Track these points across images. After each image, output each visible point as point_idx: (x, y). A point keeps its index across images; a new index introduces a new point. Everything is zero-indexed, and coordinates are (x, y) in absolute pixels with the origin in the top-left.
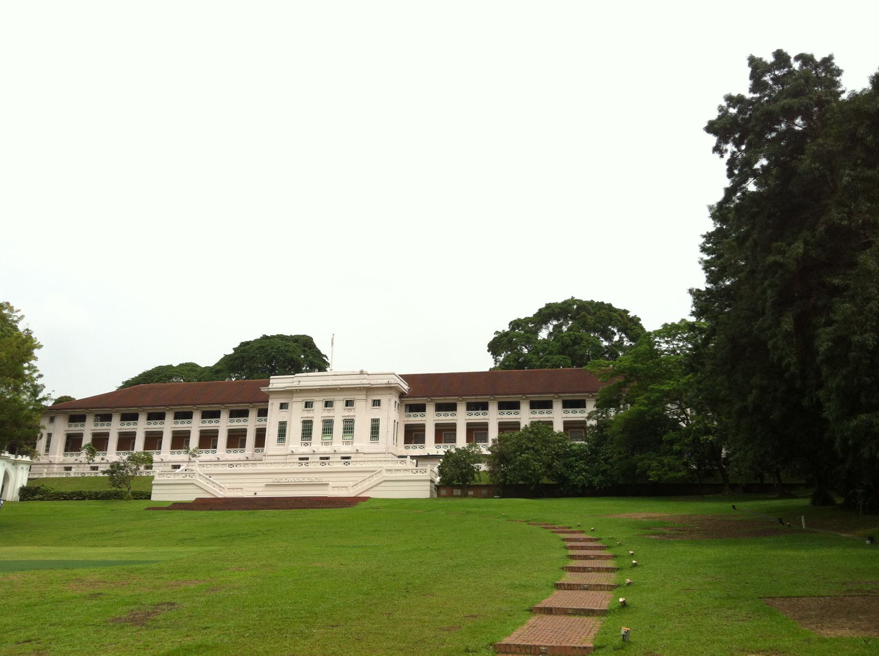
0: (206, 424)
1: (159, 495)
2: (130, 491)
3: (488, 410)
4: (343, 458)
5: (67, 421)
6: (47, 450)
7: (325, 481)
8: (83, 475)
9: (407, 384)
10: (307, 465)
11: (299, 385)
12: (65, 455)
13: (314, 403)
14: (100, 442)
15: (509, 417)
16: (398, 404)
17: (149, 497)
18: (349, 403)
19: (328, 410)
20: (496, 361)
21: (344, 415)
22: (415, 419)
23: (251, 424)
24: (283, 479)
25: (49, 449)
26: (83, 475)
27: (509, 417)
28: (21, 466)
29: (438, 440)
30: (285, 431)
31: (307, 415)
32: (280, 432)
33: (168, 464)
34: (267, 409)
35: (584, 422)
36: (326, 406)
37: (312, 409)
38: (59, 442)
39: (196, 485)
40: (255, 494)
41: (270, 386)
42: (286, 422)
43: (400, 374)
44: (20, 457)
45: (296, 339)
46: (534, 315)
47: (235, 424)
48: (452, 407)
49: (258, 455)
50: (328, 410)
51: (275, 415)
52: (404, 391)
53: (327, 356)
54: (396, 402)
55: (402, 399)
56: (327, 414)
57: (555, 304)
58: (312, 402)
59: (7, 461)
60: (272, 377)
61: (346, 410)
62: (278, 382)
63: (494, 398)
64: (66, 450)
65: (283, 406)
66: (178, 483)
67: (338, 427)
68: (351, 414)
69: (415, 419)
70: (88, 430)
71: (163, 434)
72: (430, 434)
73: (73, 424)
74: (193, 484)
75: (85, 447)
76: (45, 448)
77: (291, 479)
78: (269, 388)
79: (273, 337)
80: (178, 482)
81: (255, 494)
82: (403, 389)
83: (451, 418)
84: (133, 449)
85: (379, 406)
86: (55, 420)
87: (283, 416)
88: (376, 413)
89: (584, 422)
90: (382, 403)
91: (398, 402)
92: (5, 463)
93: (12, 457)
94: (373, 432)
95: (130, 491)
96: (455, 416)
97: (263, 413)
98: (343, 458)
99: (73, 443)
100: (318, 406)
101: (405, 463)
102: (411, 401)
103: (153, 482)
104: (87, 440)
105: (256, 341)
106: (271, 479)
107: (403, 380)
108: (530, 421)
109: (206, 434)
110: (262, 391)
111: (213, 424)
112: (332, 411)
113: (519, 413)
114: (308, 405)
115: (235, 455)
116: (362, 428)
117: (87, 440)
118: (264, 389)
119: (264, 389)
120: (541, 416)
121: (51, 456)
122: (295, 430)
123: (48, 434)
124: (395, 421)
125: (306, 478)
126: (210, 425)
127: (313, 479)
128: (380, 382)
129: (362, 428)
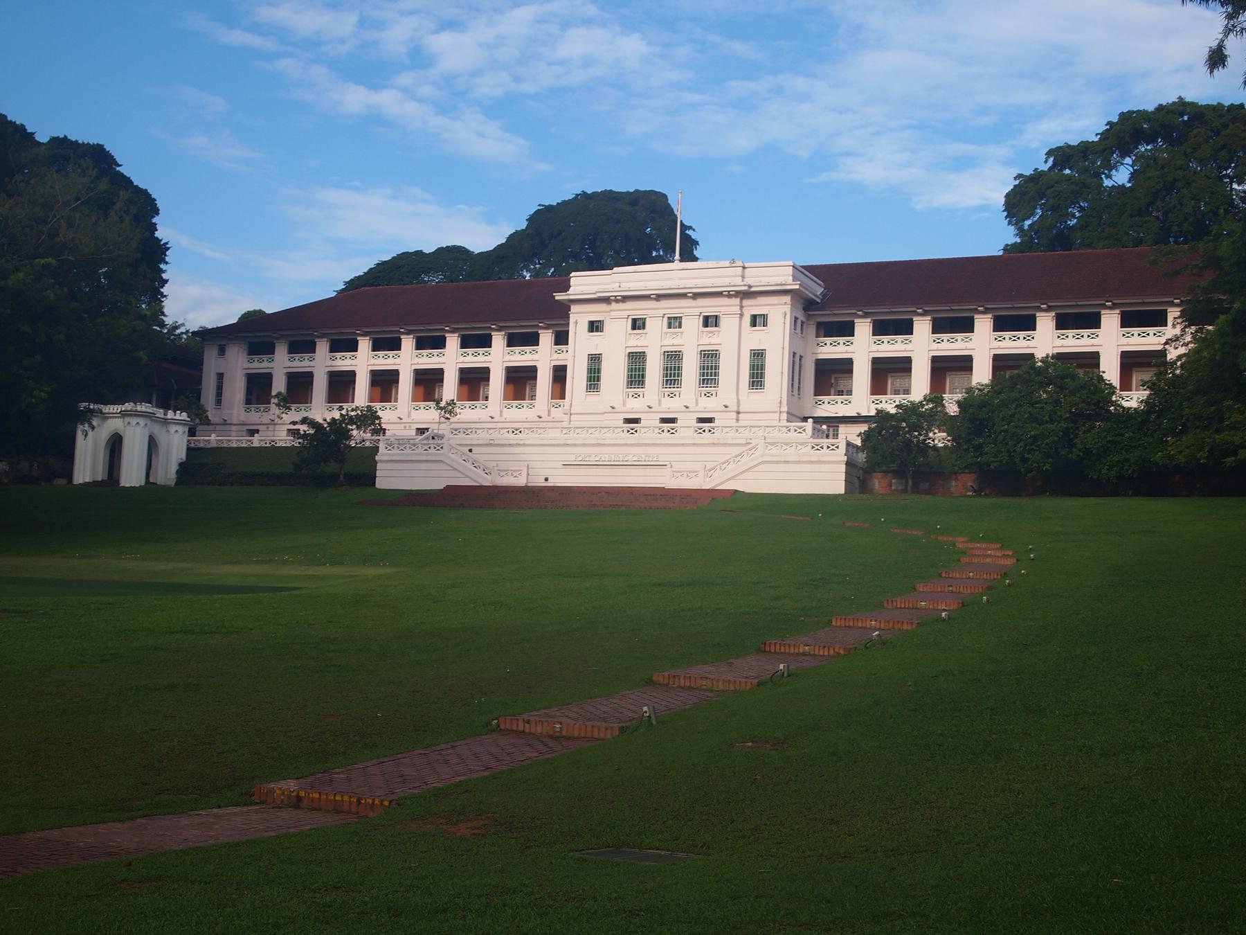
0: (468, 357)
1: (387, 480)
2: (342, 472)
3: (1034, 329)
4: (664, 420)
5: (246, 352)
6: (219, 402)
7: (663, 459)
8: (273, 443)
9: (823, 284)
10: (713, 431)
11: (619, 289)
12: (247, 410)
13: (647, 320)
14: (300, 387)
15: (1013, 344)
16: (802, 322)
17: (371, 478)
18: (710, 321)
19: (710, 332)
20: (1021, 231)
21: (703, 341)
22: (833, 349)
23: (543, 356)
24: (594, 454)
25: (221, 399)
26: (273, 443)
27: (1013, 344)
28: (173, 428)
29: (878, 387)
30: (762, 367)
31: (637, 342)
32: (761, 373)
33: (268, 428)
34: (568, 331)
35: (1163, 353)
36: (706, 324)
37: (645, 331)
38: (236, 389)
39: (446, 463)
40: (546, 479)
41: (571, 291)
42: (601, 354)
43: (801, 265)
44: (170, 414)
45: (636, 198)
46: (137, 186)
47: (470, 358)
48: (485, 342)
49: (557, 413)
50: (710, 332)
51: (581, 343)
52: (814, 297)
53: (694, 227)
54: (796, 318)
55: (809, 313)
56: (755, 339)
57: (1142, 114)
58: (645, 319)
59: (152, 420)
60: (573, 274)
61: (705, 334)
62: (583, 283)
63: (864, 312)
64: (248, 402)
65: (595, 327)
66: (398, 459)
67: (690, 368)
68: (714, 340)
69: (833, 349)
70: (281, 364)
71: (536, 371)
72: (862, 376)
73: (256, 357)
74: (440, 461)
75: (277, 396)
76: (214, 398)
77: (606, 454)
78: (569, 295)
79: (595, 194)
80: (394, 458)
81: (546, 479)
82: (807, 293)
83: (903, 347)
84: (353, 402)
85: (716, 326)
86: (227, 353)
87: (594, 343)
88: (710, 339)
89: (1163, 353)
90: (723, 321)
91: (801, 318)
92: (149, 424)
93: (160, 413)
94: (762, 370)
95: (342, 472)
96: (399, 358)
97: (561, 338)
98: (664, 420)
99: (258, 388)
100: (692, 324)
101: (804, 430)
102: (828, 316)
103: (377, 458)
104: (279, 385)
105: (564, 204)
106: (571, 455)
107: (816, 279)
108: (992, 354)
109: (471, 376)
110: (557, 300)
111: (481, 358)
112: (716, 333)
113: (910, 341)
114: (638, 324)
115: (519, 413)
116: (732, 369)
117: (279, 385)
118: (559, 297)
119: (559, 297)
120: (1076, 342)
121: (225, 412)
122: (614, 371)
123: (218, 374)
124: (794, 353)
125: (632, 454)
126: (1078, 342)
127: (643, 456)
128: (765, 280)
129: (732, 369)
